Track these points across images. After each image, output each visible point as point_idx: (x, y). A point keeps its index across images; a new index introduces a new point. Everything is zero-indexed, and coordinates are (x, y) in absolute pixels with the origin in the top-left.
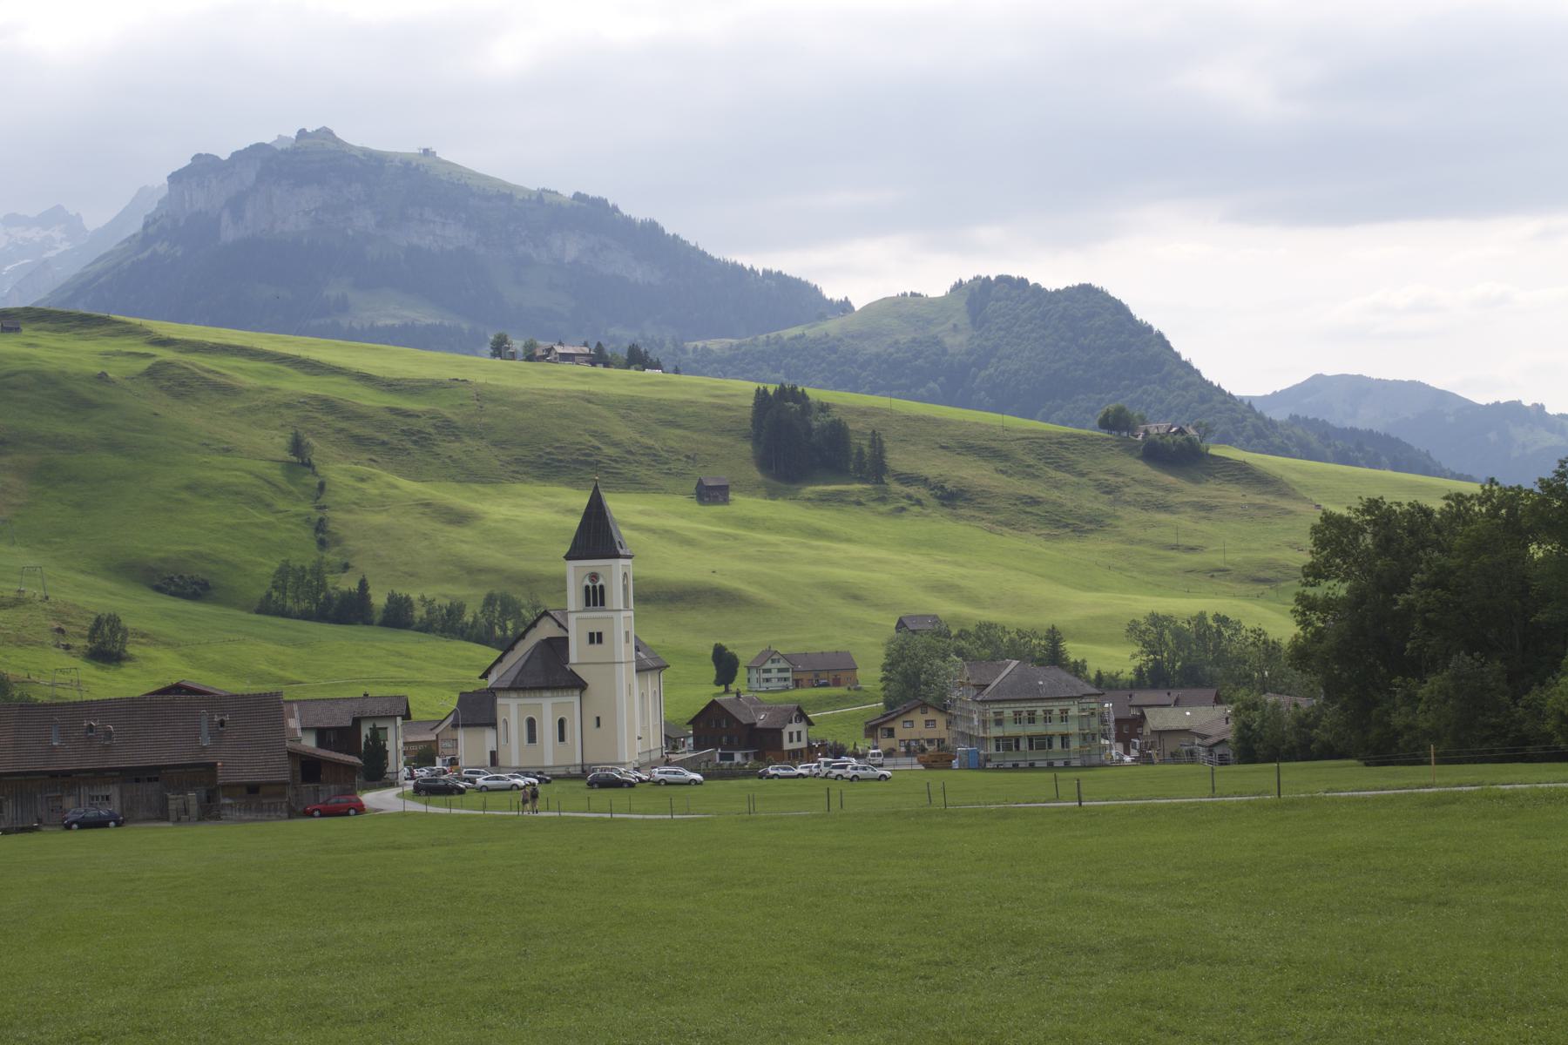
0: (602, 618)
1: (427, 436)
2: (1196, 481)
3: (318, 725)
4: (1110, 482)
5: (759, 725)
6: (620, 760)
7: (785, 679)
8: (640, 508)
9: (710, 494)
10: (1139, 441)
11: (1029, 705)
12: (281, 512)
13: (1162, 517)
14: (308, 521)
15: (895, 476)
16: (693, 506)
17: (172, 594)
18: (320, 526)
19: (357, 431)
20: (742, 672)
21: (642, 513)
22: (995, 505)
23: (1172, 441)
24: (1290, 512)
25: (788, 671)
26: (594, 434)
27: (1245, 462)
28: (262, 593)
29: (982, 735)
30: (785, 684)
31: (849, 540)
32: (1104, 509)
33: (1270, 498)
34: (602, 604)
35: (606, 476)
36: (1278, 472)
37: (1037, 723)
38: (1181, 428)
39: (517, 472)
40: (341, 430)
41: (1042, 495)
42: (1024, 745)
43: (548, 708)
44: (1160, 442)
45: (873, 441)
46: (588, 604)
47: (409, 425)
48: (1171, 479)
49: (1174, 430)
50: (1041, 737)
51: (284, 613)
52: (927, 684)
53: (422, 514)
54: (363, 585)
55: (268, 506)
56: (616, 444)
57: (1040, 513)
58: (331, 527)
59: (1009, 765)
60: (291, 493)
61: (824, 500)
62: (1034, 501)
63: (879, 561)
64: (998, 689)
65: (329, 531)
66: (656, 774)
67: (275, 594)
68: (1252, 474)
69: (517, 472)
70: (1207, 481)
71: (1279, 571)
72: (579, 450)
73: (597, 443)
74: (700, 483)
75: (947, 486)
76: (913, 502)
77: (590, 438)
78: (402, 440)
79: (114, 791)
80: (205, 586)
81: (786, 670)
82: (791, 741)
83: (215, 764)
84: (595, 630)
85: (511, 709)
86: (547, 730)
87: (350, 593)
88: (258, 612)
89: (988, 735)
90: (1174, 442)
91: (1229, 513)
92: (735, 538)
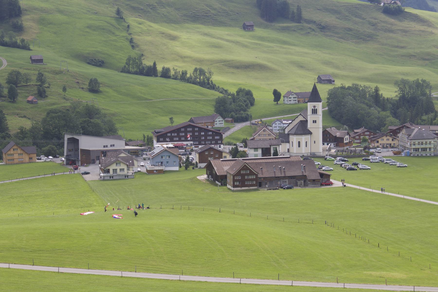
0: (314, 117)
1: (155, 6)
2: (400, 21)
3: (262, 147)
4: (373, 22)
5: (338, 136)
6: (320, 152)
7: (295, 100)
8: (227, 33)
9: (247, 27)
10: (381, 6)
11: (422, 140)
12: (118, 35)
13: (391, 35)
14: (127, 39)
15: (304, 20)
16: (243, 32)
17: (93, 65)
18: (131, 41)
19: (133, 5)
20: (282, 98)
21: (228, 35)
22: (338, 31)
23: (393, 7)
24: (433, 33)
25: (296, 98)
26: (207, 6)
27: (417, 14)
28: (123, 65)
29: (410, 148)
30: (295, 102)
31: (294, 45)
32: (373, 32)
33: (426, 27)
34: (316, 113)
35: (213, 20)
36: (428, 18)
37: (423, 145)
38: (395, 2)
39: (185, 19)
40: (127, 5)
41: (352, 27)
42: (420, 150)
43: (304, 139)
44: (389, 7)
45: (298, 9)
46: (313, 113)
47: (149, 2)
48: (393, 20)
49: (393, 2)
50: (424, 148)
51: (129, 72)
52: (344, 106)
53: (162, 36)
54: (155, 64)
55: (113, 33)
56: (215, 9)
57: (352, 34)
58: (134, 41)
59: (416, 155)
60: (119, 29)
61: (284, 29)
62: (350, 30)
63: (306, 53)
64: (414, 136)
65: (134, 43)
66: (361, 167)
67: (127, 66)
68: (419, 18)
69: (185, 19)
70: (404, 21)
71: (432, 56)
72: (204, 11)
73: (209, 9)
74: (244, 24)
75: (322, 24)
76: (311, 30)
77: (206, 7)
78: (147, 8)
79: (287, 180)
80: (103, 62)
81: (296, 98)
82: (346, 140)
83: (306, 175)
84: (315, 120)
85: (294, 139)
86: (303, 144)
87: (151, 66)
88: (122, 72)
89: (412, 148)
90: (394, 7)
91: (413, 34)
92: (260, 44)
